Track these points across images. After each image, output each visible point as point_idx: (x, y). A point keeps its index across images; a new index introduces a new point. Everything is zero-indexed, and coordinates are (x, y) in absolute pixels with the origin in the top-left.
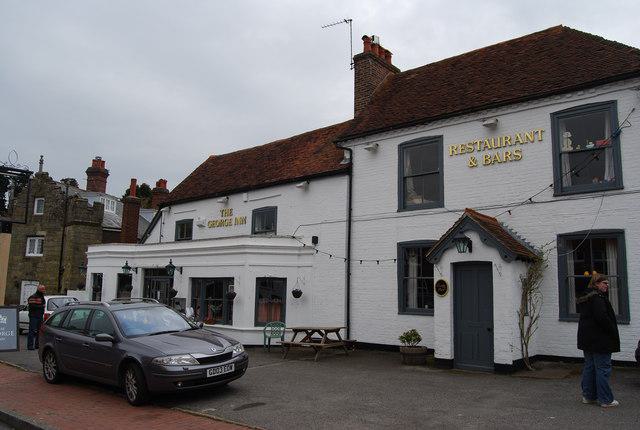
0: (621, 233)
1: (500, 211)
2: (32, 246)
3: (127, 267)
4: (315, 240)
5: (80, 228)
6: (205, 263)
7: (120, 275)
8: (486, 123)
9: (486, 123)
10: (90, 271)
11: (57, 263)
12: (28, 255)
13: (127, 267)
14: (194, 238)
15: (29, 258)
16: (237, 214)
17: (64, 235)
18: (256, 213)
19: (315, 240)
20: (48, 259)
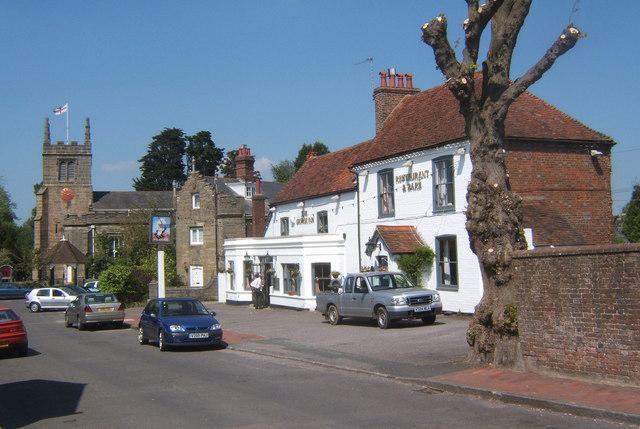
0: (437, 238)
1: (415, 221)
2: (195, 237)
3: (247, 256)
4: (345, 236)
5: (227, 220)
6: (296, 253)
7: (245, 262)
8: (37, 225)
9: (37, 225)
10: (227, 259)
11: (214, 249)
12: (192, 243)
13: (247, 256)
14: (266, 236)
15: (192, 247)
16: (309, 216)
17: (216, 226)
18: (319, 214)
19: (345, 236)
20: (208, 245)
